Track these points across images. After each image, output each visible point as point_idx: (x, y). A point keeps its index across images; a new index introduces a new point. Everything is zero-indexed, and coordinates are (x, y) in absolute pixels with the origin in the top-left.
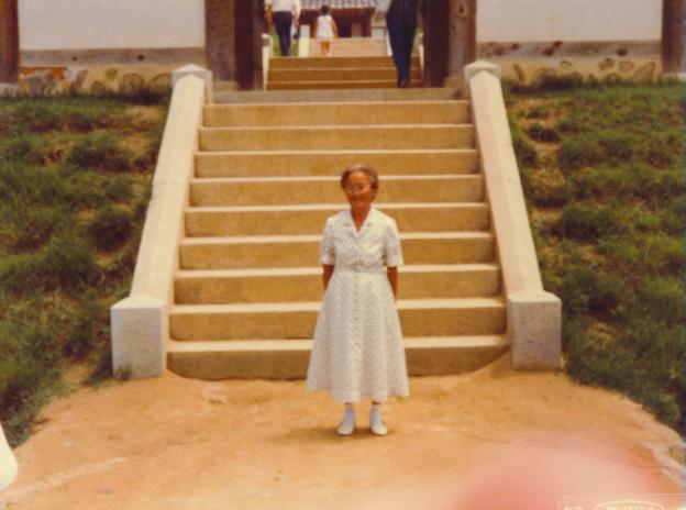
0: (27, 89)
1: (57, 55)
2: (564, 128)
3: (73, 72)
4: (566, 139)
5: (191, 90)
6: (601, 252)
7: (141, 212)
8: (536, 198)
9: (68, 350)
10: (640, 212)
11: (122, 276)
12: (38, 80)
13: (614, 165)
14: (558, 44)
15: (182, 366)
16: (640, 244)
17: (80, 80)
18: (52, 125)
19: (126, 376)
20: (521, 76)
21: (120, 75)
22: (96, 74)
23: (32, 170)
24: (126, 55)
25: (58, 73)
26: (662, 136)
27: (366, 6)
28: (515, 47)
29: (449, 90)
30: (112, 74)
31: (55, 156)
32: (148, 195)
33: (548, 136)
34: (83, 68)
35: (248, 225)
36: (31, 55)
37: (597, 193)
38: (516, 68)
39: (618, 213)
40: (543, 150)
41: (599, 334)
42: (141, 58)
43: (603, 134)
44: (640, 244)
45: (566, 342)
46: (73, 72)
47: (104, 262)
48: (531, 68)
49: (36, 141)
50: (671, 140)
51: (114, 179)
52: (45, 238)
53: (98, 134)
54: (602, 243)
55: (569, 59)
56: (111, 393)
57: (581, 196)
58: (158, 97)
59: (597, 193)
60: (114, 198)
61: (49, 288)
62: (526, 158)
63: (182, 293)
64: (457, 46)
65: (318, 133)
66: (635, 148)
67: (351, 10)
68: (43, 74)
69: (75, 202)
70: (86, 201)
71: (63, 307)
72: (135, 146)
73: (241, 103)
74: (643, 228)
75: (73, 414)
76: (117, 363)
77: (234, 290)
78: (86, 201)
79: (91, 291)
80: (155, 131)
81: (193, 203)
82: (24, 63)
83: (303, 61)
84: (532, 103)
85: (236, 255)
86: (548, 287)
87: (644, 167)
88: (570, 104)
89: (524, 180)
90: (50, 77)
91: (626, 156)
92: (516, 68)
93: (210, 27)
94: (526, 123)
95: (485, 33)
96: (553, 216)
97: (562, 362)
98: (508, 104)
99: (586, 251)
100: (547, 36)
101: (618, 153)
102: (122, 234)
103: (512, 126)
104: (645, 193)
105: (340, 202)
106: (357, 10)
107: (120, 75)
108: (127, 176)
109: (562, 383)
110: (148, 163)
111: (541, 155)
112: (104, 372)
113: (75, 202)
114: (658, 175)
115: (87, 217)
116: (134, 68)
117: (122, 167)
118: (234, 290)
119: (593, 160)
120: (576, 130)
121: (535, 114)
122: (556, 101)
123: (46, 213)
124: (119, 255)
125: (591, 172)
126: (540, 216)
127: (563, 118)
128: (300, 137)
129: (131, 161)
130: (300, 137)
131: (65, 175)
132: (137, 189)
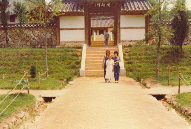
0: (61, 47)
1: (65, 42)
2: (129, 52)
3: (67, 44)
4: (130, 53)
5: (85, 47)
6: (132, 65)
7: (81, 61)
8: (125, 59)
9: (74, 74)
10: (137, 61)
11: (80, 67)
12: (62, 45)
13: (135, 56)
14: (131, 40)
15: (86, 76)
16: (136, 64)
17: (68, 45)
18: (68, 51)
19: (81, 76)
20: (127, 45)
21: (73, 45)
22: (70, 45)
23: (68, 56)
24: (74, 42)
25: (65, 44)
26: (141, 52)
27: (107, 26)
28: (126, 41)
29: (116, 47)
30: (72, 45)
31: (70, 55)
32: (81, 59)
33: (127, 53)
34: (69, 44)
35: (92, 62)
36: (61, 42)
37: (132, 59)
38: (126, 44)
39: (134, 61)
40: (127, 54)
41: (130, 73)
42: (76, 42)
43: (134, 52)
44: (136, 64)
45: (126, 74)
46: (67, 44)
47: (77, 66)
48: (128, 44)
49: (67, 53)
50: (142, 53)
51: (77, 57)
52: (70, 64)
53: (74, 52)
54: (132, 64)
55: (133, 42)
56: (79, 78)
57: (130, 59)
58: (81, 48)
59: (132, 59)
60: (77, 59)
61: (71, 69)
62: (124, 55)
63: (86, 69)
64: (118, 41)
65: (100, 52)
66: (138, 54)
67: (103, 27)
68: (63, 45)
69: (73, 60)
70: (74, 60)
71: (73, 71)
72: (79, 54)
73: (91, 48)
74: (137, 63)
75: (75, 81)
76: (80, 75)
77: (91, 69)
78: (74, 60)
79: (76, 69)
80: (81, 52)
81: (86, 60)
82: (61, 43)
83: (95, 41)
84: (126, 48)
85: (91, 65)
86: (125, 68)
87: (138, 56)
88: (131, 49)
89: (124, 57)
90: (64, 45)
91: (136, 55)
92: (126, 44)
93: (85, 38)
94: (125, 51)
95: (122, 39)
96: (127, 61)
97: (126, 75)
98: (123, 49)
99: (130, 65)
100: (130, 39)
101: (135, 54)
102: (79, 63)
103: (123, 51)
104: (138, 59)
105: (102, 70)
106: (105, 27)
107: (73, 45)
108: (78, 57)
109: (126, 77)
110: (81, 55)
111: (126, 55)
112: (79, 76)
113: (73, 60)
114: (140, 57)
115: (74, 61)
116: (75, 44)
117: (77, 56)
118: (91, 69)
119: (132, 55)
120: (131, 52)
121: (126, 50)
122: (129, 48)
123: (70, 61)
124: (79, 65)
125: (132, 57)
126: (125, 61)
127: (129, 50)
128: (98, 53)
129: (79, 55)
130: (98, 53)
131: (71, 57)
132: (80, 59)
